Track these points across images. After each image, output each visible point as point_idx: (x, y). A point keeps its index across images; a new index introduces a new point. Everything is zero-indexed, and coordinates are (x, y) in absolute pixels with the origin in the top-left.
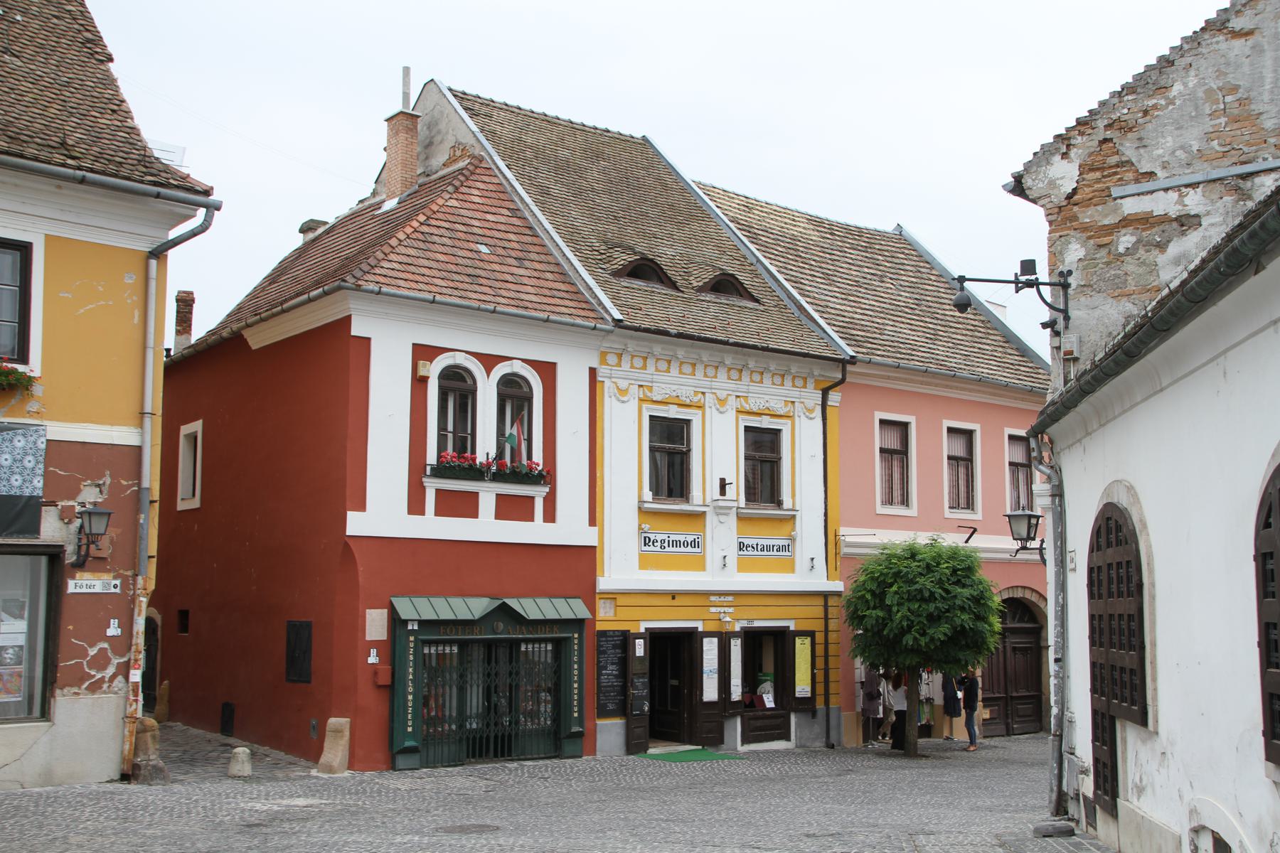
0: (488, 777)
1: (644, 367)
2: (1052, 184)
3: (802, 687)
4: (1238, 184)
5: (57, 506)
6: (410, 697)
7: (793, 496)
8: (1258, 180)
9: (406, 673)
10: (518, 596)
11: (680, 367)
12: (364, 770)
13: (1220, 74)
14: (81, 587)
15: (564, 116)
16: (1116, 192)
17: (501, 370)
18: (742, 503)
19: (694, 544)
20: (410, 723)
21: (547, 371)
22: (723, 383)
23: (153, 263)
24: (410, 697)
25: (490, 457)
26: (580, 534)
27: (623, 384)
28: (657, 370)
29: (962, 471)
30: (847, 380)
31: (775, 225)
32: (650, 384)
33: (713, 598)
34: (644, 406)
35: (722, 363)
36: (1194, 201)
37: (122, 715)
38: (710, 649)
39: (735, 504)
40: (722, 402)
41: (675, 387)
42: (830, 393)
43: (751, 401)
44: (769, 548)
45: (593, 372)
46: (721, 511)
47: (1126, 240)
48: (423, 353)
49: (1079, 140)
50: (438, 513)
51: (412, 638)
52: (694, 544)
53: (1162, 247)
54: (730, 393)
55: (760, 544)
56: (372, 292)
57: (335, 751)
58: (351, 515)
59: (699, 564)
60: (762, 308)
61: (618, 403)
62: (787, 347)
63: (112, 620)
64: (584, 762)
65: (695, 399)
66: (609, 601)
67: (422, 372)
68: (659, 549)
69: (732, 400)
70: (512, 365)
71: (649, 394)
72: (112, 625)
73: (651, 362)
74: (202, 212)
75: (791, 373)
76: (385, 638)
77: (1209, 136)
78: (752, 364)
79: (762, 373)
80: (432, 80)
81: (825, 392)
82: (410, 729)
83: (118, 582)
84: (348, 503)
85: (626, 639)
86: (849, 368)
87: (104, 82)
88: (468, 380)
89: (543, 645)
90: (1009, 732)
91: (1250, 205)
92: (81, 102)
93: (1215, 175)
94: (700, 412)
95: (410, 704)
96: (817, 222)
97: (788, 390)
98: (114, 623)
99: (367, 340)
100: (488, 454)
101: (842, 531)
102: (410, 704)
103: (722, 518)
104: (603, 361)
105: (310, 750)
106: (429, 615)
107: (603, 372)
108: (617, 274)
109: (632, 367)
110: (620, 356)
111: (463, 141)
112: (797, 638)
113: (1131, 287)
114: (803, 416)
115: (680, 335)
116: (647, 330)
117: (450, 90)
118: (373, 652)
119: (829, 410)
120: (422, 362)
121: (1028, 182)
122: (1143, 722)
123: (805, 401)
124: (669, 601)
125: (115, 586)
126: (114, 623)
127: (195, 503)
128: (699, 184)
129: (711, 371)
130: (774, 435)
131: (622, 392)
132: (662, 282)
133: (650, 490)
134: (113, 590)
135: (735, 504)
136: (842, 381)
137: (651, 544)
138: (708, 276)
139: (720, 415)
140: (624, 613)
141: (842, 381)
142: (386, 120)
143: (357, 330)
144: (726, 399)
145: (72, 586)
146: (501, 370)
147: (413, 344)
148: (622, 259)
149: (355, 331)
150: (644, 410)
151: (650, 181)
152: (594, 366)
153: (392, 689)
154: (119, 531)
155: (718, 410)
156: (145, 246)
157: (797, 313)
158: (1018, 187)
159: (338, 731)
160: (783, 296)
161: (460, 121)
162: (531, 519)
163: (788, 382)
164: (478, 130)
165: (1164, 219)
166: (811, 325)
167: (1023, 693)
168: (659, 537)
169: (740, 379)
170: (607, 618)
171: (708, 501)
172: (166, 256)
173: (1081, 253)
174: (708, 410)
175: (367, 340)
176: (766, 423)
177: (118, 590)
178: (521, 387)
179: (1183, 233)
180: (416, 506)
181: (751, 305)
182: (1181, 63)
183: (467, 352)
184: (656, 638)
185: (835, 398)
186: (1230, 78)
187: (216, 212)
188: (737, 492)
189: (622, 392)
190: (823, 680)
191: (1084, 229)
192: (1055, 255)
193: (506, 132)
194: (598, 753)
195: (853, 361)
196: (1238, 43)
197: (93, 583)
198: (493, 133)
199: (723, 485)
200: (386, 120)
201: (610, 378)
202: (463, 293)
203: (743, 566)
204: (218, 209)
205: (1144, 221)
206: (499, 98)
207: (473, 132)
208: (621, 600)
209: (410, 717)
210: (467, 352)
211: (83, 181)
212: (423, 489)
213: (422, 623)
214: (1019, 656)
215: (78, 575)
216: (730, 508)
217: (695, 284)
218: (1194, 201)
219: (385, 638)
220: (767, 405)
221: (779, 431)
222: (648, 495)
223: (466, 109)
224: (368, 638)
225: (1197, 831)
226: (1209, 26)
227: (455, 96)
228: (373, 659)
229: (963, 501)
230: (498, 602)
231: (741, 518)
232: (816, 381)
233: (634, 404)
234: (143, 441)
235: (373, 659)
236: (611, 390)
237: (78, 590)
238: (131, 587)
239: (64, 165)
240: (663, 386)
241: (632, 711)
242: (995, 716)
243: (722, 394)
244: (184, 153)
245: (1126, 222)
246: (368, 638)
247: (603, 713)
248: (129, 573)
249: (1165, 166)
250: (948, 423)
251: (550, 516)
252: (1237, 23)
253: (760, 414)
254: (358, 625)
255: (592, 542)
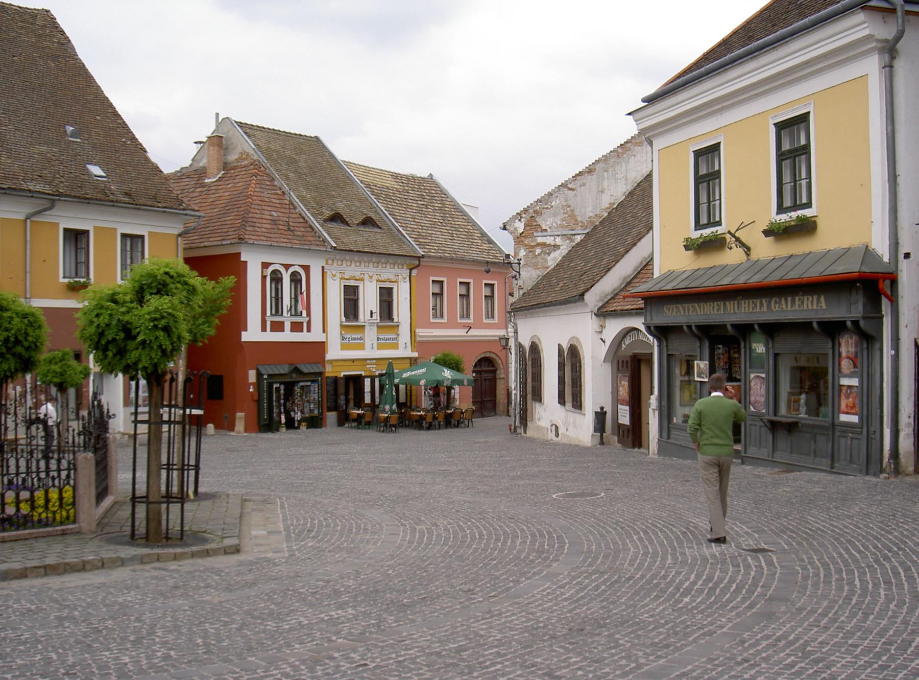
1: (342, 265)
2: (516, 229)
4: (570, 237)
8: (576, 237)
12: (251, 432)
13: (566, 201)
16: (535, 234)
17: (291, 270)
18: (379, 321)
19: (361, 339)
21: (306, 268)
22: (371, 269)
26: (315, 335)
27: (334, 272)
31: (379, 182)
33: (368, 361)
35: (354, 259)
36: (558, 241)
38: (367, 382)
40: (371, 277)
44: (389, 339)
45: (323, 267)
46: (371, 324)
47: (538, 251)
48: (265, 265)
49: (524, 216)
50: (271, 331)
52: (361, 339)
53: (549, 254)
55: (371, 335)
57: (240, 425)
58: (243, 333)
59: (362, 347)
64: (324, 429)
67: (265, 274)
73: (344, 263)
90: (483, 416)
91: (574, 244)
93: (564, 233)
96: (396, 176)
101: (417, 330)
103: (372, 327)
104: (327, 263)
105: (231, 428)
106: (271, 372)
107: (327, 267)
108: (325, 221)
110: (333, 260)
113: (540, 266)
115: (358, 251)
116: (346, 250)
117: (236, 122)
118: (252, 387)
119: (412, 278)
121: (508, 227)
122: (541, 401)
124: (351, 363)
128: (344, 162)
130: (390, 290)
131: (334, 276)
132: (343, 222)
136: (419, 265)
140: (336, 369)
141: (419, 265)
146: (291, 270)
148: (328, 213)
149: (242, 259)
151: (325, 164)
153: (259, 401)
157: (397, 232)
158: (505, 228)
160: (390, 224)
165: (550, 245)
166: (405, 240)
167: (488, 399)
168: (348, 337)
170: (330, 371)
173: (525, 253)
175: (246, 262)
176: (387, 285)
179: (555, 250)
180: (264, 329)
181: (379, 230)
182: (555, 195)
184: (348, 378)
185: (414, 272)
188: (376, 316)
189: (334, 276)
191: (526, 245)
192: (516, 253)
196: (570, 192)
199: (372, 313)
203: (380, 347)
205: (543, 245)
208: (335, 364)
211: (165, 212)
212: (266, 321)
213: (269, 375)
214: (487, 382)
218: (558, 241)
222: (344, 319)
223: (245, 133)
225: (552, 426)
226: (562, 185)
229: (465, 316)
231: (378, 327)
234: (780, 416)
235: (251, 390)
243: (371, 274)
245: (539, 245)
247: (329, 410)
249: (550, 228)
250: (459, 280)
251: (309, 330)
252: (570, 186)
254: (246, 376)
255: (324, 340)
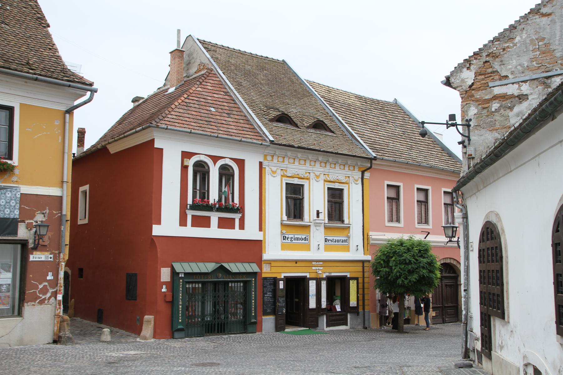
0: (215, 341)
1: (283, 161)
2: (463, 81)
3: (353, 302)
4: (545, 81)
5: (25, 222)
6: (180, 307)
7: (349, 218)
8: (553, 79)
9: (179, 296)
10: (228, 262)
11: (299, 161)
12: (160, 338)
13: (537, 32)
14: (36, 258)
15: (248, 51)
16: (491, 84)
17: (220, 163)
18: (327, 221)
19: (305, 239)
20: (180, 318)
21: (241, 163)
22: (318, 169)
23: (67, 115)
24: (180, 307)
25: (215, 201)
26: (255, 235)
27: (274, 169)
28: (289, 163)
29: (423, 207)
30: (373, 167)
31: (341, 99)
32: (286, 169)
33: (314, 263)
34: (283, 178)
35: (318, 159)
36: (525, 89)
37: (54, 315)
38: (312, 285)
39: (323, 222)
40: (318, 177)
41: (297, 170)
42: (365, 173)
43: (330, 176)
44: (338, 241)
45: (261, 163)
46: (317, 225)
47: (495, 106)
48: (186, 155)
49: (475, 62)
50: (193, 226)
51: (181, 281)
52: (305, 239)
53: (511, 108)
54: (321, 173)
55: (334, 239)
56: (164, 128)
57: (148, 330)
58: (154, 227)
59: (307, 248)
60: (335, 135)
61: (272, 177)
62: (346, 153)
63: (49, 273)
64: (257, 335)
65: (306, 176)
66: (268, 264)
67: (185, 164)
68: (290, 241)
69: (322, 176)
70: (225, 161)
71: (285, 173)
72: (49, 275)
73: (286, 159)
74: (89, 93)
75: (348, 164)
76: (169, 281)
77: (532, 60)
78: (331, 160)
79: (335, 164)
80: (190, 35)
81: (363, 173)
82: (180, 321)
83: (52, 256)
84: (153, 221)
85: (275, 281)
86: (374, 162)
87: (46, 36)
88: (206, 167)
89: (239, 284)
90: (444, 322)
91: (550, 90)
92: (36, 45)
93: (534, 77)
94: (308, 181)
95: (180, 310)
96: (359, 98)
97: (347, 172)
98: (50, 274)
99: (162, 150)
100: (214, 200)
101: (371, 233)
102: (180, 310)
103: (318, 228)
104: (265, 159)
105: (136, 330)
106: (189, 270)
107: (265, 164)
108: (271, 120)
109: (278, 161)
110: (273, 156)
111: (204, 62)
112: (350, 281)
113: (498, 126)
114: (353, 183)
115: (299, 147)
116: (285, 145)
117: (198, 39)
118: (164, 287)
119: (364, 180)
120: (185, 159)
121: (452, 80)
122: (503, 317)
123: (354, 176)
124: (294, 264)
125: (51, 258)
126: (50, 274)
127: (86, 221)
128: (307, 81)
129: (313, 163)
130: (340, 191)
131: (274, 172)
132: (291, 124)
133: (286, 215)
134: (50, 260)
135: (323, 222)
136: (371, 167)
137: (286, 239)
138: (312, 121)
139: (317, 182)
140: (274, 270)
141: (371, 167)
142: (170, 53)
143: (157, 145)
144: (319, 175)
145: (32, 258)
146: (220, 163)
147: (182, 151)
148: (274, 114)
149: (156, 146)
150: (283, 180)
151: (286, 80)
152: (261, 161)
153: (172, 303)
154: (52, 233)
155: (316, 180)
156: (64, 108)
157: (351, 138)
158: (448, 82)
159: (149, 321)
160: (344, 130)
161: (202, 53)
162: (234, 228)
163: (347, 168)
164: (210, 57)
165: (512, 96)
166: (357, 143)
167: (450, 305)
168: (290, 236)
169: (325, 167)
170: (267, 272)
171: (311, 220)
172: (73, 112)
173: (476, 111)
174: (311, 180)
175: (162, 150)
176: (337, 186)
177: (52, 260)
178: (229, 170)
179: (520, 103)
180: (183, 222)
181: (330, 134)
182: (519, 28)
183: (205, 155)
184: (289, 281)
185: (367, 175)
186: (541, 34)
187: (95, 93)
188: (324, 216)
189: (274, 172)
190: (362, 299)
191: (477, 100)
192: (464, 112)
193: (222, 58)
194: (263, 331)
195: (375, 159)
196: (545, 19)
197: (41, 256)
198: (217, 58)
199: (318, 213)
200: (170, 53)
201: (268, 166)
202: (204, 129)
203: (327, 249)
204: (96, 92)
205: (503, 97)
206: (219, 43)
207: (208, 58)
208: (273, 264)
209: (180, 315)
210: (205, 155)
211: (36, 79)
212: (186, 215)
213: (186, 274)
214: (448, 288)
215: (34, 253)
216: (321, 223)
217: (306, 125)
218: (525, 89)
219: (169, 281)
220: (337, 178)
221: (343, 189)
222: (285, 218)
223: (205, 48)
224: (162, 280)
225: (526, 365)
226: (532, 11)
227: (200, 42)
228: (164, 290)
229: (423, 220)
230: (219, 265)
231: (326, 228)
232: (359, 168)
233: (279, 177)
234: (63, 194)
235: (164, 290)
236: (269, 171)
237: (34, 260)
238: (58, 258)
239: (28, 73)
240: (292, 170)
241: (278, 313)
242: (438, 315)
243: (318, 173)
244: (81, 67)
245: (495, 98)
246: (162, 280)
247: (265, 313)
248: (57, 252)
249: (512, 73)
250: (417, 186)
251: (242, 227)
252: (544, 10)
253: (334, 182)
254: (158, 275)
255: (261, 238)
